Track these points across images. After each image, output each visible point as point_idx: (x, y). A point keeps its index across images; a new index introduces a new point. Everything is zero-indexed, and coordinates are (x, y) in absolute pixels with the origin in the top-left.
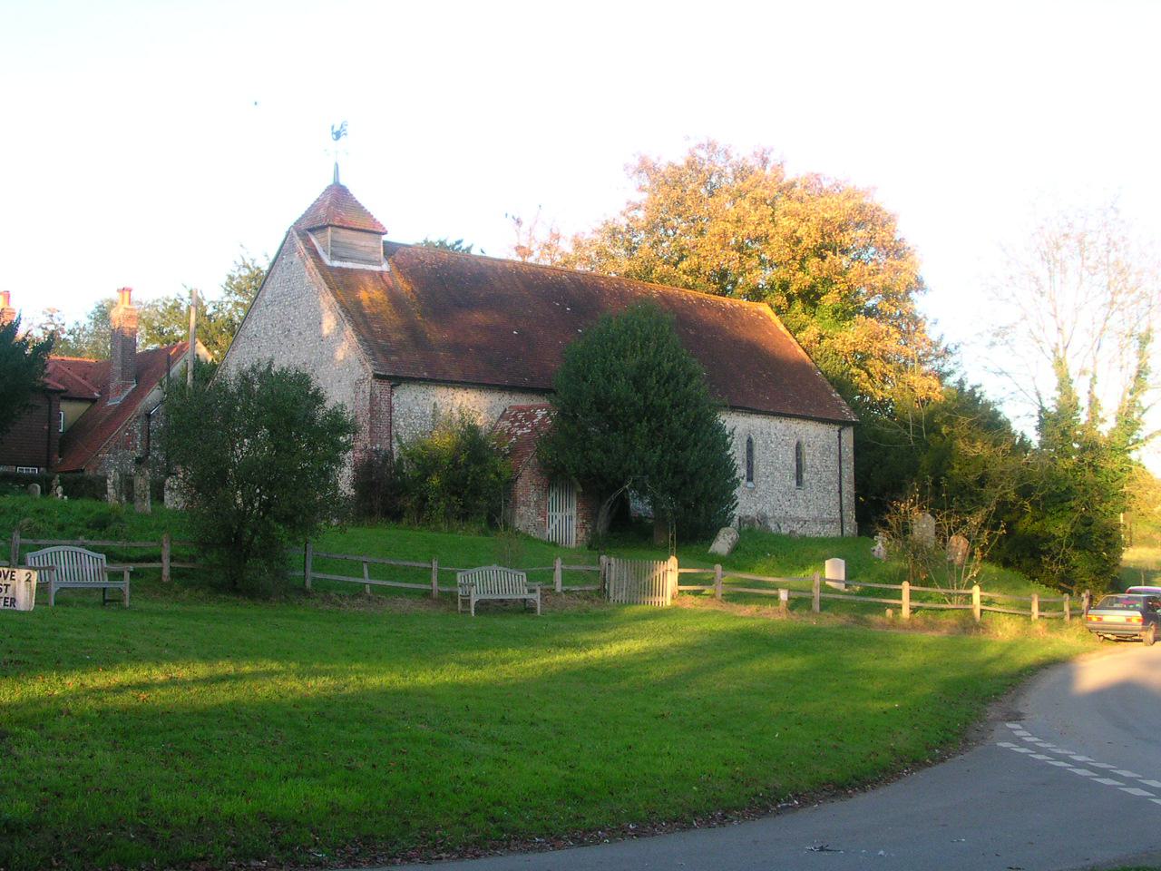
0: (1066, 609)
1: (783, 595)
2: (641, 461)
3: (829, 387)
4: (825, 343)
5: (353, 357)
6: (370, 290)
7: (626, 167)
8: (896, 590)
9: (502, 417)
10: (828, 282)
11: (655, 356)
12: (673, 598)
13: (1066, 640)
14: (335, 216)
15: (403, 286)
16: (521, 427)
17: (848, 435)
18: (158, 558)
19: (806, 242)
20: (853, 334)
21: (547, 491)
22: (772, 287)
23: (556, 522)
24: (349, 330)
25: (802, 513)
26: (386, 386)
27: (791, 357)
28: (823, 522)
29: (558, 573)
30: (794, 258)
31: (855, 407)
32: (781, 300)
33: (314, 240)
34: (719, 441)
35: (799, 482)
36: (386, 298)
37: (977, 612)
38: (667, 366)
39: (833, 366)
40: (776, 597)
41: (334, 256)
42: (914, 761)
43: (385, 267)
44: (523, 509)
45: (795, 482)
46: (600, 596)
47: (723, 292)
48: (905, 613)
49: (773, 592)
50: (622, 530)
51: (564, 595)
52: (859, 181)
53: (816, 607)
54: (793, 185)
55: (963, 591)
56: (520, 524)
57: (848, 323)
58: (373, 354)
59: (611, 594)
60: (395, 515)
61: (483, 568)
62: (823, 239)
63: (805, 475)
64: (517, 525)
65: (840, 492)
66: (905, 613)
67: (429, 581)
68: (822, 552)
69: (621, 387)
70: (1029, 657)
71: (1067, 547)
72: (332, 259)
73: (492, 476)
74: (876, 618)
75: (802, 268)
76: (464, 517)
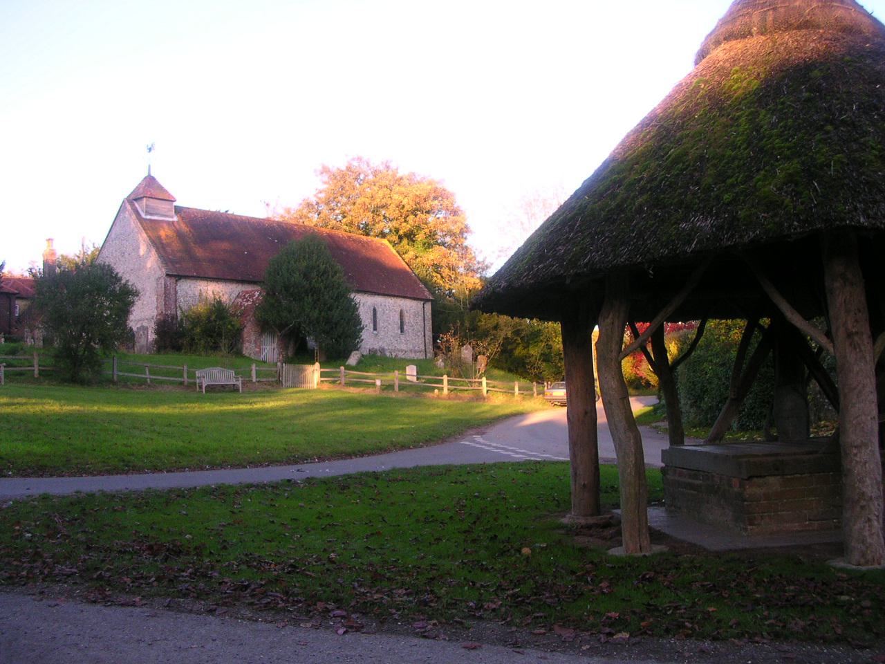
0: (535, 390)
1: (378, 383)
2: (308, 316)
3: (418, 282)
4: (418, 260)
5: (156, 266)
6: (166, 230)
7: (315, 171)
8: (440, 379)
9: (238, 296)
10: (419, 228)
11: (316, 262)
12: (318, 384)
13: (527, 405)
14: (150, 190)
15: (184, 228)
16: (247, 301)
17: (428, 306)
18: (33, 366)
19: (408, 207)
20: (433, 255)
21: (261, 335)
22: (391, 231)
23: (266, 351)
24: (153, 251)
25: (404, 347)
26: (173, 280)
27: (398, 266)
28: (415, 352)
29: (254, 373)
30: (401, 216)
31: (433, 293)
32: (395, 238)
33: (137, 205)
34: (353, 308)
35: (402, 331)
36: (175, 235)
37: (485, 391)
38: (322, 267)
39: (421, 272)
40: (374, 384)
41: (147, 213)
42: (402, 446)
43: (175, 219)
44: (247, 344)
45: (400, 331)
46: (277, 384)
47: (368, 235)
48: (446, 391)
49: (373, 381)
50: (301, 354)
51: (257, 384)
52: (436, 175)
53: (396, 388)
54: (401, 178)
55: (477, 380)
56: (246, 352)
57: (431, 250)
58: (166, 264)
59: (284, 383)
60: (177, 348)
61: (206, 369)
62: (416, 205)
63: (405, 327)
64: (244, 352)
65: (424, 336)
66: (446, 391)
67: (182, 376)
68: (407, 363)
69: (296, 278)
70: (508, 411)
71: (539, 360)
72: (146, 215)
73: (229, 326)
74: (430, 394)
75: (405, 221)
76: (216, 347)
